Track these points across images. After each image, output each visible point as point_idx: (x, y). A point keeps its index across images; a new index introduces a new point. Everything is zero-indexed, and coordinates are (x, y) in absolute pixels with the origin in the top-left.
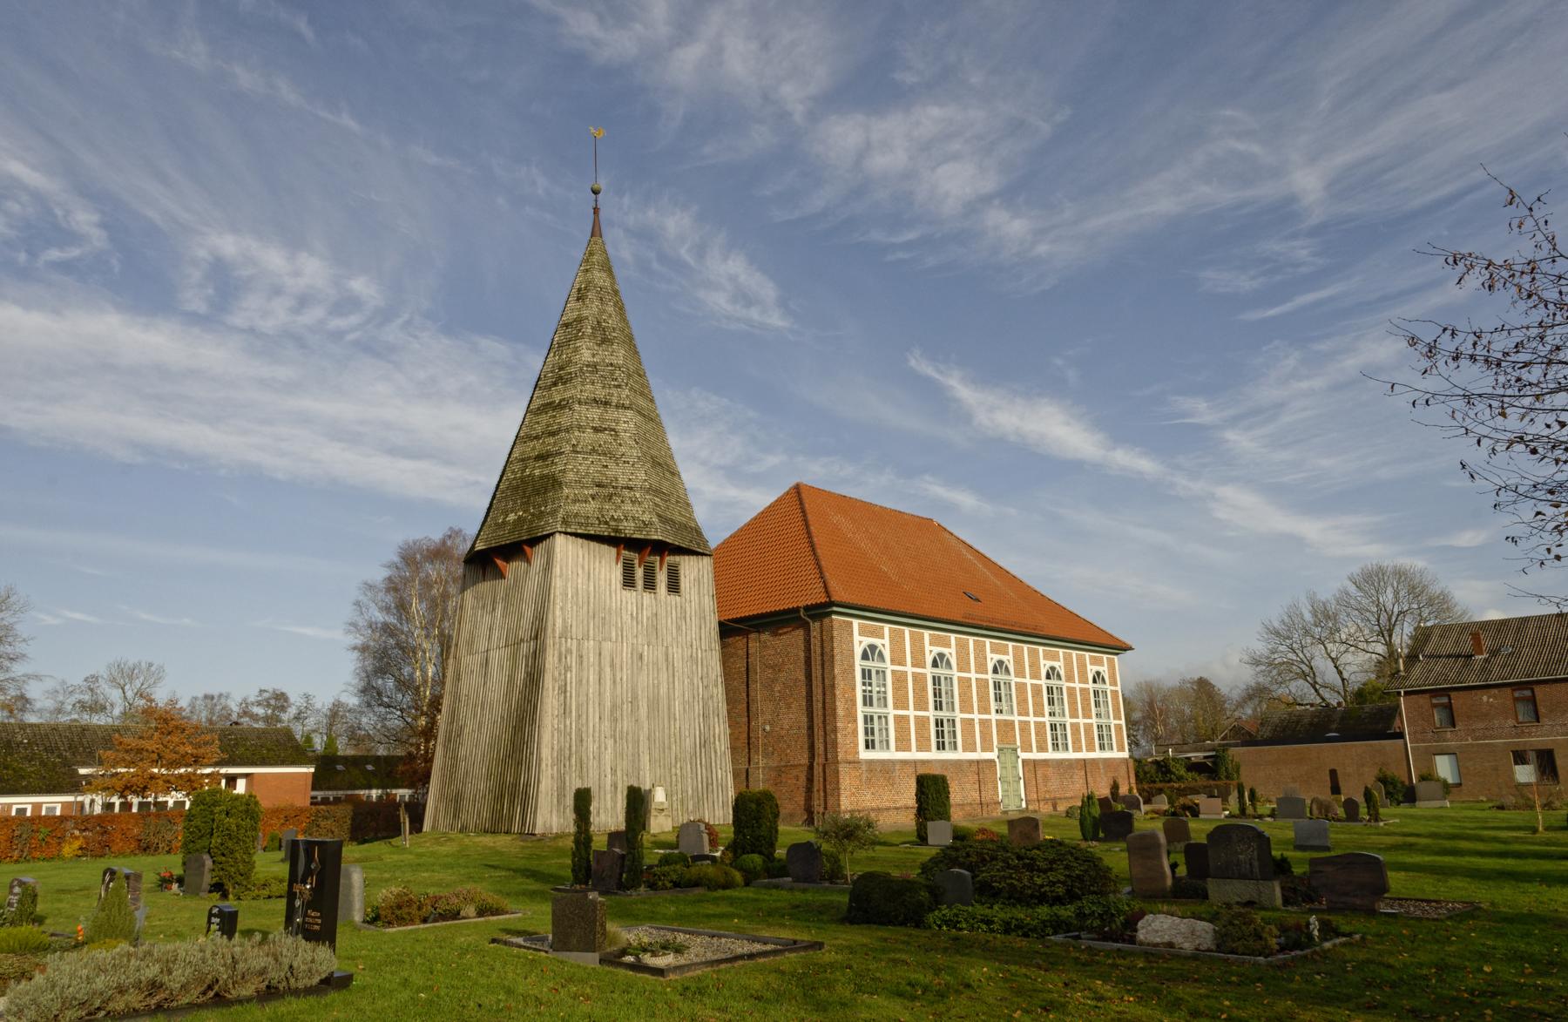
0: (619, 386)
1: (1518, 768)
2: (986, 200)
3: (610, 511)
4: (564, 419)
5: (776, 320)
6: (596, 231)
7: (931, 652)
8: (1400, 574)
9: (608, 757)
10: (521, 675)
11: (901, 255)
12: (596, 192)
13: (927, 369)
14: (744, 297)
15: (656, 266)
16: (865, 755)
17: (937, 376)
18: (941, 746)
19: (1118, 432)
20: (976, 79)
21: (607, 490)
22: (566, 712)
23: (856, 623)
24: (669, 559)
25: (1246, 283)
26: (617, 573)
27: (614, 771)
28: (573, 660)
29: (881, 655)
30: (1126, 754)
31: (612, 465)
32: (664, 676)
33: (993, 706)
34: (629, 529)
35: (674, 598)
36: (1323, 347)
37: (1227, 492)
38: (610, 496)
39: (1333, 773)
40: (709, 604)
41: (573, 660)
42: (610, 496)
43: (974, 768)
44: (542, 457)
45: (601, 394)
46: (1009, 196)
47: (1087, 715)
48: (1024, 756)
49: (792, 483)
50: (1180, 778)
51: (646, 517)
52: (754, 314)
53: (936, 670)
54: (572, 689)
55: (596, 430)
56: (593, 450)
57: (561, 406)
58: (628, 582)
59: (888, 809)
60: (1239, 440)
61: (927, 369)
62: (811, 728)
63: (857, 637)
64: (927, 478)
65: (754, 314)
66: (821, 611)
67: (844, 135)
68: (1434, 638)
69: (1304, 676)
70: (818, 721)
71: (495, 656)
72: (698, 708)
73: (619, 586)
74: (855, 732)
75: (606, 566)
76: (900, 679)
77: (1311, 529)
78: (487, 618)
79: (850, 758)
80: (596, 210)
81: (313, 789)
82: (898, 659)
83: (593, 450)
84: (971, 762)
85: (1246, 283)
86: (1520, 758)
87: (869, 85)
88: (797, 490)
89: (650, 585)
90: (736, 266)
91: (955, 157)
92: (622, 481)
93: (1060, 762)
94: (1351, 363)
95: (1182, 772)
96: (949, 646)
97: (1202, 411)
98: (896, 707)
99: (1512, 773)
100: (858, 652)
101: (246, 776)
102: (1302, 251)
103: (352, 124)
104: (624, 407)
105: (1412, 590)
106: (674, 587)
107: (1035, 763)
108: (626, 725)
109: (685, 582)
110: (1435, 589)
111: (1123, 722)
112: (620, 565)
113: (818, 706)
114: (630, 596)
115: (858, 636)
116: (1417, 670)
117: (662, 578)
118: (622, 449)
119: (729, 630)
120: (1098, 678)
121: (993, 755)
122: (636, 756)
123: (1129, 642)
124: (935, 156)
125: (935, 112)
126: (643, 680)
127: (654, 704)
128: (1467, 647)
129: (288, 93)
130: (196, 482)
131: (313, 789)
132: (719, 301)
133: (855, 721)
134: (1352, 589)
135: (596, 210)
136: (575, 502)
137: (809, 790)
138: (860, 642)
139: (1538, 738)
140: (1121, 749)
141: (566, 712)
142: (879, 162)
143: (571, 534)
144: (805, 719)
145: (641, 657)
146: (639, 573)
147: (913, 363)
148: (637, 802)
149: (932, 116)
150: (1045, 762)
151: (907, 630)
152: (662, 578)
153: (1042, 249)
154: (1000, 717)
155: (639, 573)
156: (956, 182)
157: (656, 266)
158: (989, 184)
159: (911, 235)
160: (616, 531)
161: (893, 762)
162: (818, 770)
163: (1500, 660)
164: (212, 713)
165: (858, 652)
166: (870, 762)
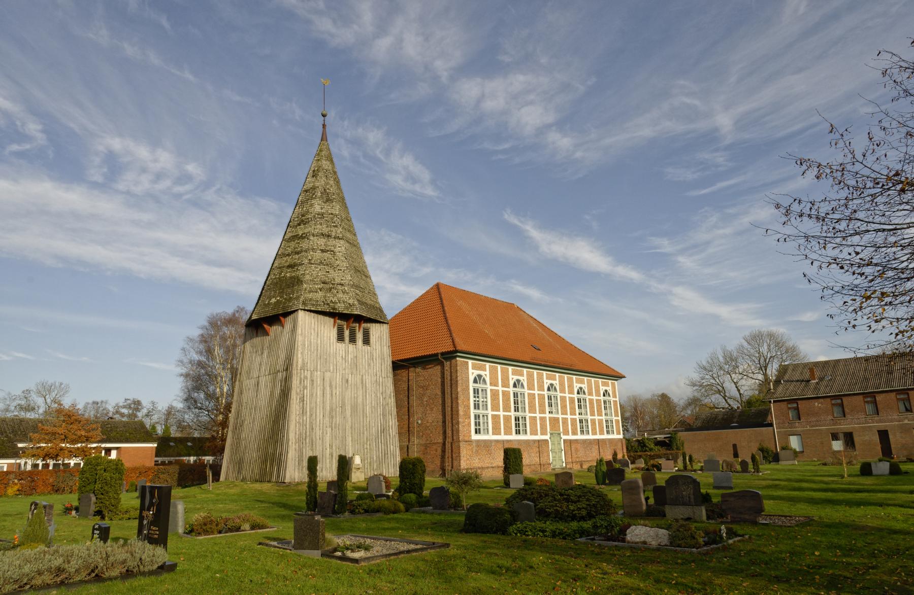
0: (336, 226)
1: (834, 443)
2: (548, 127)
3: (331, 297)
4: (304, 245)
5: (430, 192)
6: (324, 138)
7: (512, 378)
8: (771, 335)
9: (328, 438)
10: (278, 391)
11: (501, 157)
12: (324, 116)
13: (514, 220)
14: (412, 179)
15: (362, 160)
16: (475, 437)
17: (519, 224)
18: (608, 432)
19: (620, 257)
20: (544, 60)
21: (329, 286)
22: (303, 413)
23: (470, 362)
24: (364, 325)
25: (690, 175)
26: (334, 333)
27: (331, 447)
28: (308, 383)
29: (484, 380)
30: (621, 436)
31: (331, 271)
32: (360, 393)
33: (577, 411)
34: (341, 308)
35: (366, 348)
36: (731, 211)
37: (679, 290)
38: (330, 289)
39: (735, 446)
40: (387, 351)
41: (308, 383)
42: (330, 289)
43: (536, 444)
44: (291, 266)
45: (325, 230)
46: (560, 125)
47: (600, 414)
48: (564, 437)
49: (435, 283)
50: (651, 450)
51: (351, 301)
52: (417, 188)
53: (476, 385)
54: (307, 399)
55: (323, 251)
56: (321, 262)
57: (302, 237)
58: (340, 338)
59: (488, 468)
60: (686, 262)
61: (514, 220)
62: (444, 422)
63: (471, 370)
64: (513, 281)
65: (417, 188)
66: (450, 355)
67: (469, 90)
68: (789, 371)
69: (719, 392)
70: (448, 418)
71: (263, 380)
72: (380, 410)
73: (335, 340)
74: (469, 424)
75: (327, 329)
76: (495, 394)
77: (724, 311)
78: (258, 359)
79: (466, 439)
80: (324, 126)
81: (156, 456)
82: (494, 383)
83: (321, 262)
84: (534, 441)
85: (690, 175)
86: (835, 437)
87: (485, 62)
88: (437, 286)
89: (353, 340)
90: (408, 161)
91: (531, 103)
92: (338, 280)
93: (585, 441)
94: (746, 220)
95: (652, 446)
96: (522, 375)
97: (665, 245)
98: (493, 410)
99: (830, 446)
100: (471, 379)
101: (117, 448)
102: (720, 158)
103: (191, 77)
104: (339, 238)
105: (777, 344)
106: (366, 341)
107: (571, 441)
108: (338, 420)
109: (373, 338)
110: (790, 344)
111: (620, 418)
112: (336, 329)
113: (448, 409)
114: (341, 346)
115: (471, 369)
116: (780, 389)
117: (360, 336)
118: (338, 262)
119: (397, 366)
120: (606, 393)
121: (547, 437)
122: (344, 438)
123: (620, 370)
124: (520, 102)
125: (521, 78)
126: (348, 394)
127: (354, 408)
128: (807, 376)
129: (154, 59)
130: (51, 275)
131: (156, 456)
132: (398, 180)
133: (470, 418)
134: (745, 344)
135: (324, 126)
136: (310, 292)
137: (443, 457)
138: (472, 373)
139: (844, 426)
140: (618, 433)
141: (303, 413)
142: (489, 105)
143: (308, 311)
144: (441, 417)
145: (347, 381)
146: (347, 333)
147: (506, 216)
148: (344, 464)
149: (519, 80)
150: (576, 441)
151: (499, 366)
152: (360, 336)
153: (578, 154)
154: (551, 415)
155: (347, 333)
156: (531, 117)
157: (362, 160)
158: (550, 118)
159: (506, 146)
160: (334, 309)
161: (491, 441)
162: (448, 446)
163: (824, 383)
164: (97, 412)
165: (471, 379)
166: (478, 441)
